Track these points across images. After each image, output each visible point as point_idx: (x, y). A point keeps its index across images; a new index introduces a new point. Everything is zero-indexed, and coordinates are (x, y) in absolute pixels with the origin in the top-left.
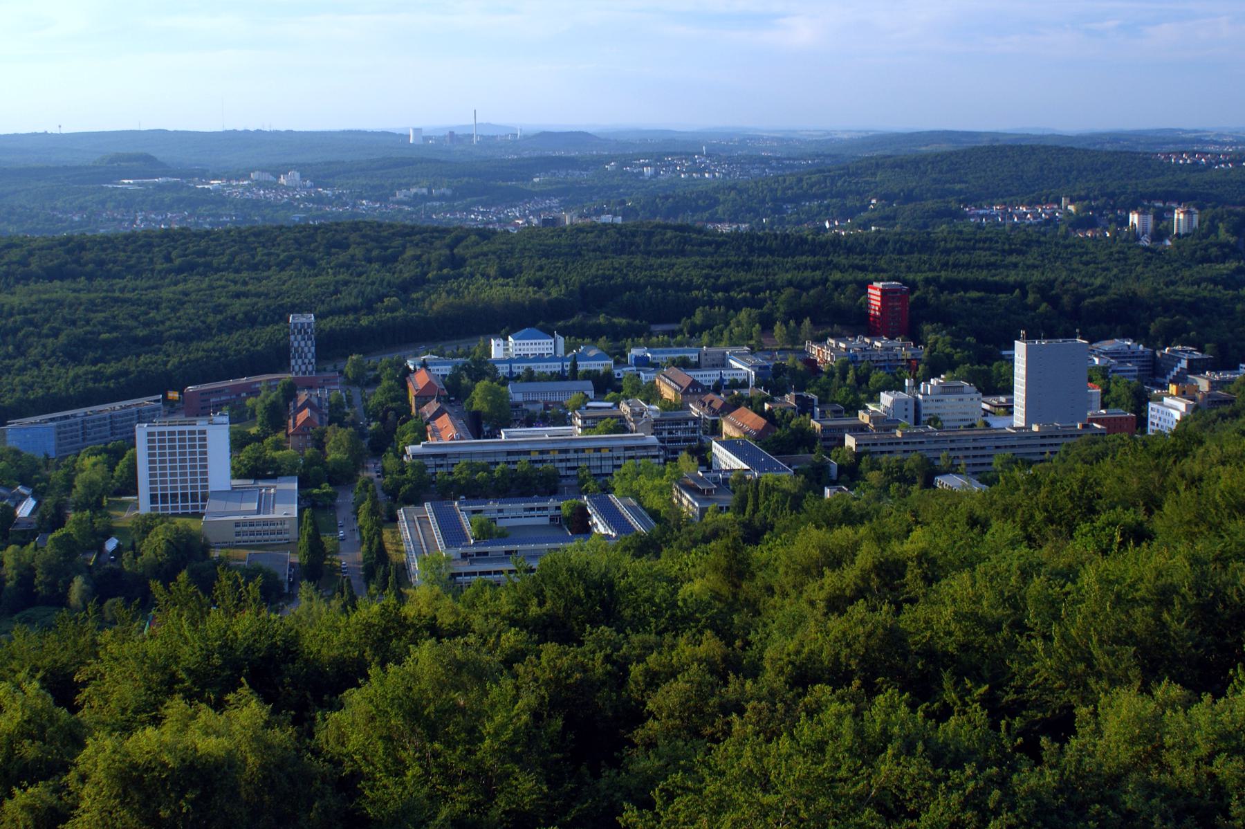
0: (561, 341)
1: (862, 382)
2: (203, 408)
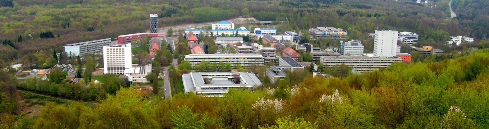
2: (124, 42)
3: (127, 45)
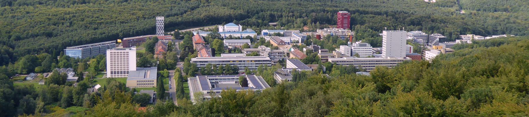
0: (241, 27)
1: (336, 41)
2: (127, 45)
3: (132, 48)
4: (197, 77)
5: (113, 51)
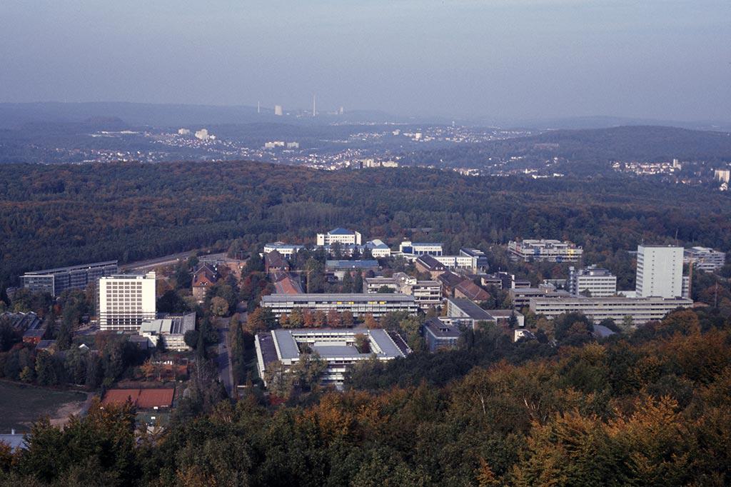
4: (272, 331)
5: (111, 280)
